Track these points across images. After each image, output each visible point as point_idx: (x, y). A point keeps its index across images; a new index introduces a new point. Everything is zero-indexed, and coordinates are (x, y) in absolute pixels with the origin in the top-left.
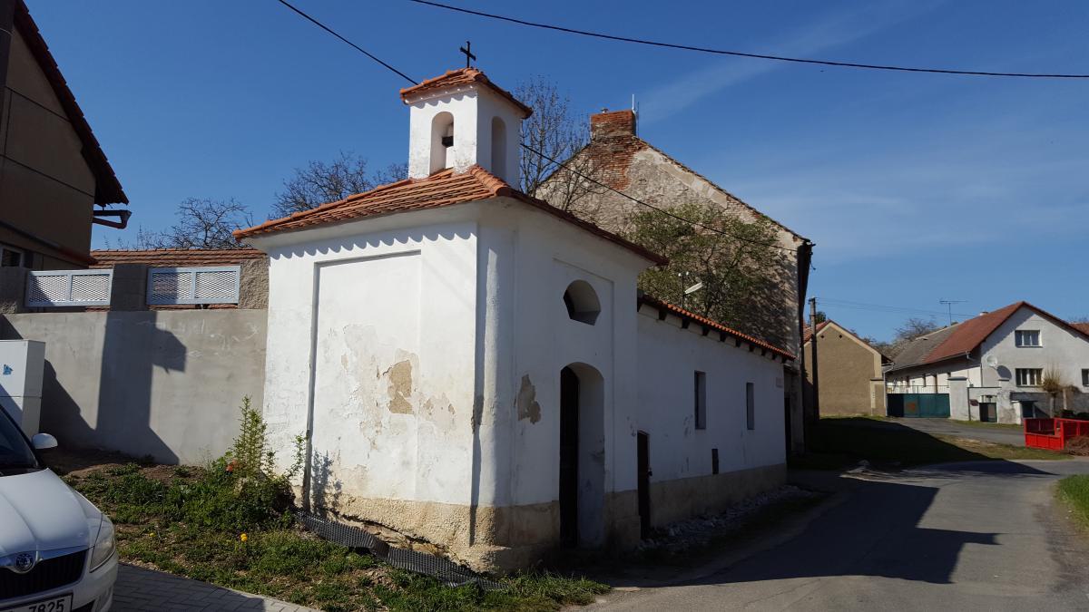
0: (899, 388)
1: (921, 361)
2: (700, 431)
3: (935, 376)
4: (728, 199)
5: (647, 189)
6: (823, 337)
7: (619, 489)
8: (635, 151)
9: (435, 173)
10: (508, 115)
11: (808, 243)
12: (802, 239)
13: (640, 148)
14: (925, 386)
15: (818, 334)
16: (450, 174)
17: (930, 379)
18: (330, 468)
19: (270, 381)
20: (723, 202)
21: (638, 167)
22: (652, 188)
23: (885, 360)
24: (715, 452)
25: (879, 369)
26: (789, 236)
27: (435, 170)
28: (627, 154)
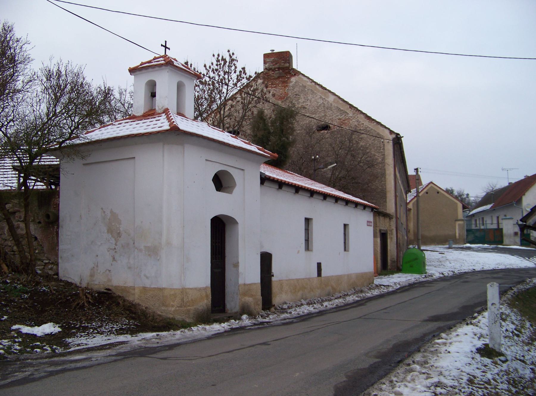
2: (346, 252)
3: (492, 217)
4: (350, 108)
5: (300, 101)
6: (427, 193)
7: (248, 282)
13: (295, 75)
14: (492, 224)
18: (234, 57)
19: (62, 227)
21: (294, 87)
22: (303, 100)
24: (319, 265)
26: (387, 132)
27: (145, 112)
28: (287, 78)
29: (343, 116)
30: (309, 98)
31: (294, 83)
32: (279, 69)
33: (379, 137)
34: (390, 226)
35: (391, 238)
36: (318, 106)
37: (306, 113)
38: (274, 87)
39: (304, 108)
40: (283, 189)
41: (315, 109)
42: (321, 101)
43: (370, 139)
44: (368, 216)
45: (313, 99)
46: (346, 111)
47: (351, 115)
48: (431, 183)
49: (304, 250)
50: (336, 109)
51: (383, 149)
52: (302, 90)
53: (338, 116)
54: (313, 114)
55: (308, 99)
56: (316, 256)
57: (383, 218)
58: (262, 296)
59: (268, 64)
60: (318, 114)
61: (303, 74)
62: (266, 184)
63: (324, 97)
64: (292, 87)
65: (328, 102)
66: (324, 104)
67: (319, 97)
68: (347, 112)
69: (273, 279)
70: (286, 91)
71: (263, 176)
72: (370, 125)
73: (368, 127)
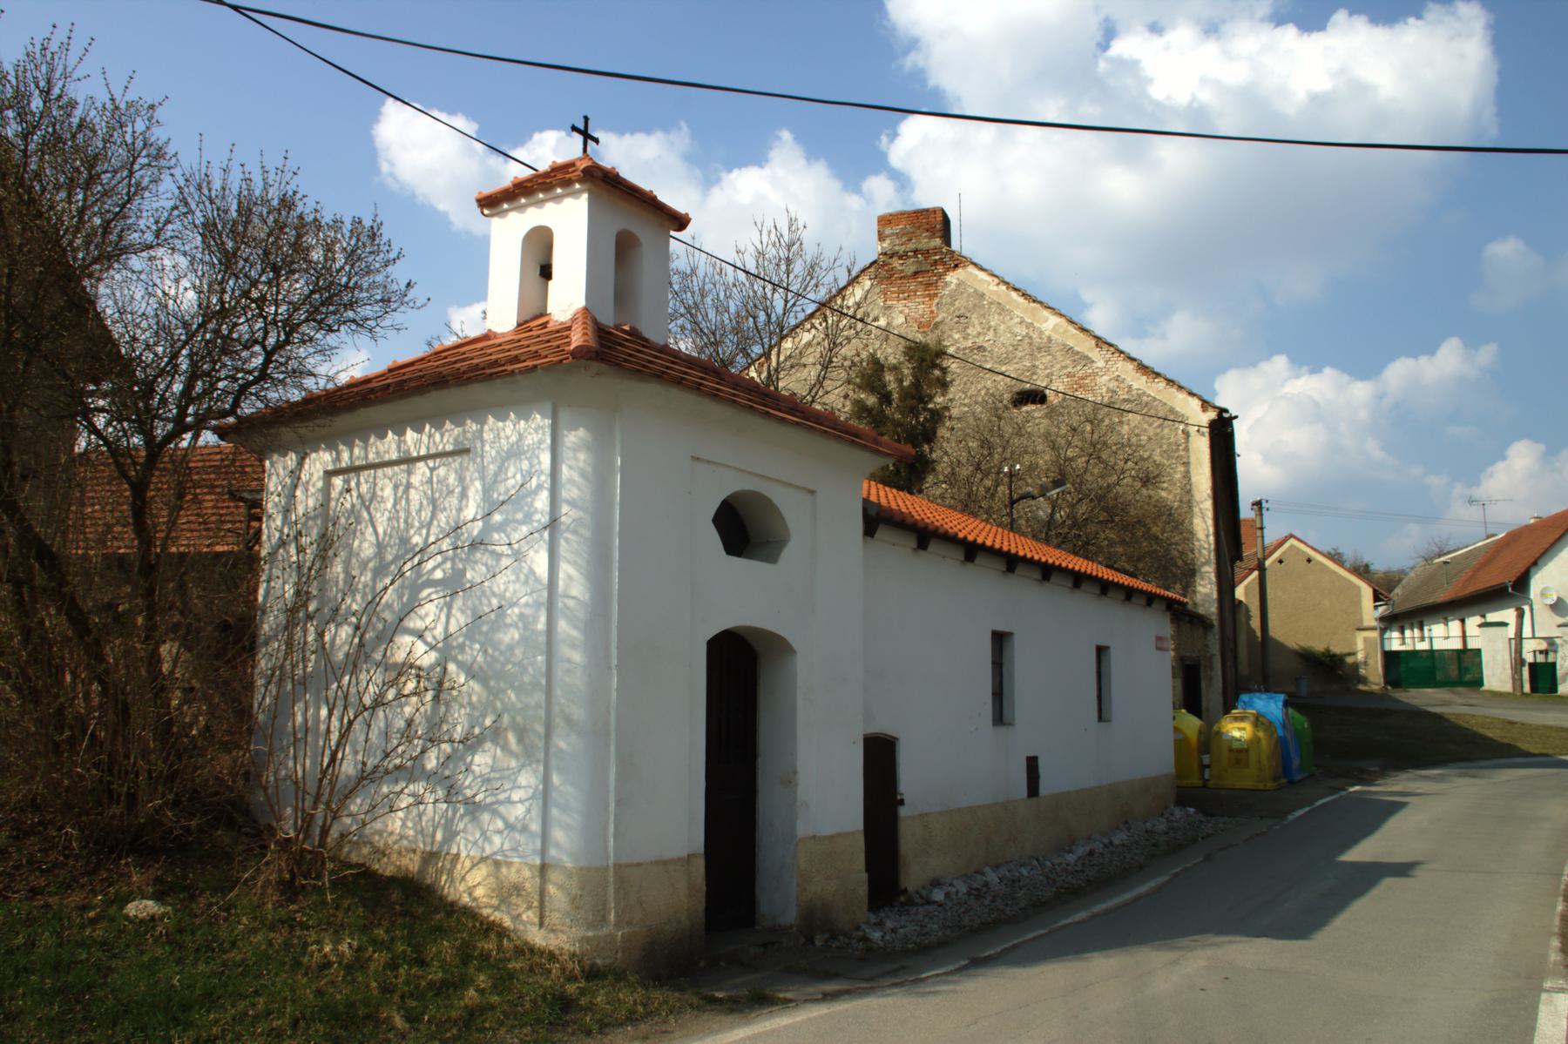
0: (1395, 642)
1: (1440, 596)
2: (1102, 724)
3: (1463, 621)
5: (969, 331)
6: (1281, 562)
7: (827, 829)
8: (948, 270)
9: (526, 322)
10: (626, 219)
11: (1226, 415)
12: (1215, 407)
13: (956, 266)
15: (1268, 563)
16: (547, 322)
17: (1455, 626)
20: (1090, 350)
21: (953, 297)
23: (1377, 597)
24: (1032, 763)
25: (1370, 612)
26: (1195, 404)
29: (1079, 368)
30: (992, 323)
31: (953, 286)
32: (916, 251)
33: (1173, 417)
34: (1207, 646)
35: (1211, 679)
36: (1015, 343)
37: (986, 361)
38: (905, 299)
39: (981, 348)
40: (1052, 580)
41: (1007, 353)
42: (1022, 331)
43: (1151, 425)
44: (1158, 625)
45: (1002, 327)
46: (1086, 353)
47: (1101, 364)
48: (1292, 536)
49: (991, 722)
50: (1062, 350)
51: (1184, 450)
52: (975, 305)
53: (1066, 367)
54: (1002, 363)
55: (990, 327)
56: (1024, 737)
57: (1188, 625)
58: (867, 870)
59: (888, 241)
60: (1017, 363)
61: (975, 265)
62: (882, 533)
63: (1029, 321)
64: (951, 296)
65: (1041, 333)
66: (1031, 338)
67: (1018, 320)
68: (1090, 356)
69: (903, 812)
70: (934, 308)
71: (873, 512)
72: (1149, 388)
73: (1144, 393)
